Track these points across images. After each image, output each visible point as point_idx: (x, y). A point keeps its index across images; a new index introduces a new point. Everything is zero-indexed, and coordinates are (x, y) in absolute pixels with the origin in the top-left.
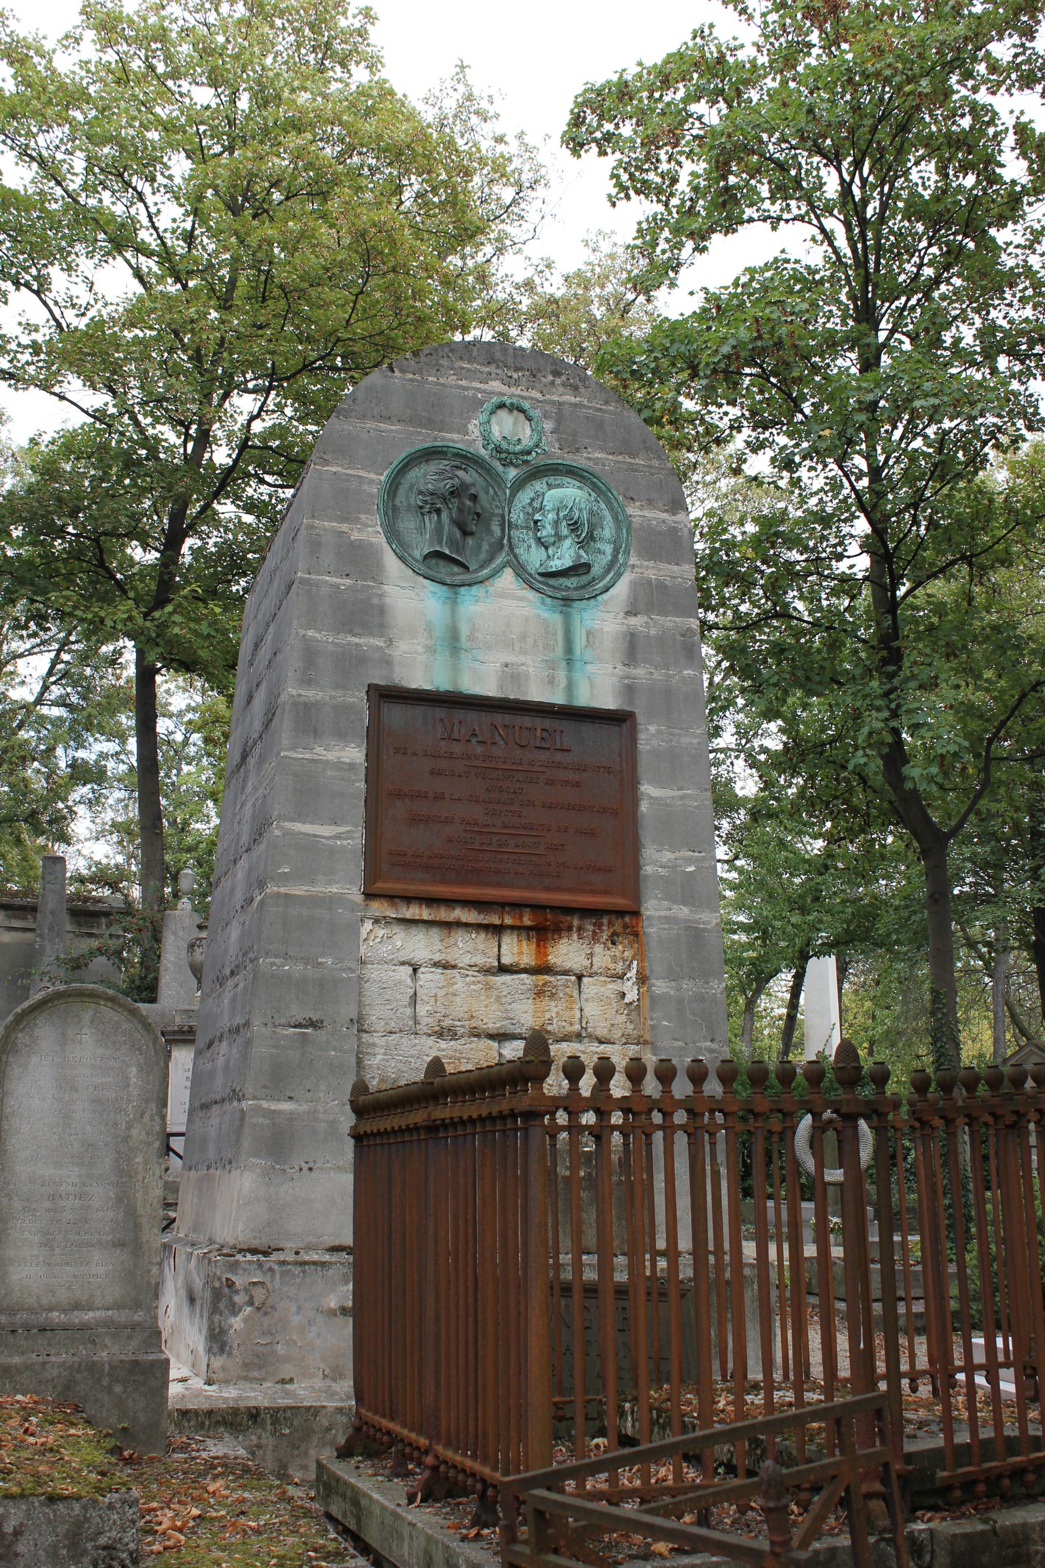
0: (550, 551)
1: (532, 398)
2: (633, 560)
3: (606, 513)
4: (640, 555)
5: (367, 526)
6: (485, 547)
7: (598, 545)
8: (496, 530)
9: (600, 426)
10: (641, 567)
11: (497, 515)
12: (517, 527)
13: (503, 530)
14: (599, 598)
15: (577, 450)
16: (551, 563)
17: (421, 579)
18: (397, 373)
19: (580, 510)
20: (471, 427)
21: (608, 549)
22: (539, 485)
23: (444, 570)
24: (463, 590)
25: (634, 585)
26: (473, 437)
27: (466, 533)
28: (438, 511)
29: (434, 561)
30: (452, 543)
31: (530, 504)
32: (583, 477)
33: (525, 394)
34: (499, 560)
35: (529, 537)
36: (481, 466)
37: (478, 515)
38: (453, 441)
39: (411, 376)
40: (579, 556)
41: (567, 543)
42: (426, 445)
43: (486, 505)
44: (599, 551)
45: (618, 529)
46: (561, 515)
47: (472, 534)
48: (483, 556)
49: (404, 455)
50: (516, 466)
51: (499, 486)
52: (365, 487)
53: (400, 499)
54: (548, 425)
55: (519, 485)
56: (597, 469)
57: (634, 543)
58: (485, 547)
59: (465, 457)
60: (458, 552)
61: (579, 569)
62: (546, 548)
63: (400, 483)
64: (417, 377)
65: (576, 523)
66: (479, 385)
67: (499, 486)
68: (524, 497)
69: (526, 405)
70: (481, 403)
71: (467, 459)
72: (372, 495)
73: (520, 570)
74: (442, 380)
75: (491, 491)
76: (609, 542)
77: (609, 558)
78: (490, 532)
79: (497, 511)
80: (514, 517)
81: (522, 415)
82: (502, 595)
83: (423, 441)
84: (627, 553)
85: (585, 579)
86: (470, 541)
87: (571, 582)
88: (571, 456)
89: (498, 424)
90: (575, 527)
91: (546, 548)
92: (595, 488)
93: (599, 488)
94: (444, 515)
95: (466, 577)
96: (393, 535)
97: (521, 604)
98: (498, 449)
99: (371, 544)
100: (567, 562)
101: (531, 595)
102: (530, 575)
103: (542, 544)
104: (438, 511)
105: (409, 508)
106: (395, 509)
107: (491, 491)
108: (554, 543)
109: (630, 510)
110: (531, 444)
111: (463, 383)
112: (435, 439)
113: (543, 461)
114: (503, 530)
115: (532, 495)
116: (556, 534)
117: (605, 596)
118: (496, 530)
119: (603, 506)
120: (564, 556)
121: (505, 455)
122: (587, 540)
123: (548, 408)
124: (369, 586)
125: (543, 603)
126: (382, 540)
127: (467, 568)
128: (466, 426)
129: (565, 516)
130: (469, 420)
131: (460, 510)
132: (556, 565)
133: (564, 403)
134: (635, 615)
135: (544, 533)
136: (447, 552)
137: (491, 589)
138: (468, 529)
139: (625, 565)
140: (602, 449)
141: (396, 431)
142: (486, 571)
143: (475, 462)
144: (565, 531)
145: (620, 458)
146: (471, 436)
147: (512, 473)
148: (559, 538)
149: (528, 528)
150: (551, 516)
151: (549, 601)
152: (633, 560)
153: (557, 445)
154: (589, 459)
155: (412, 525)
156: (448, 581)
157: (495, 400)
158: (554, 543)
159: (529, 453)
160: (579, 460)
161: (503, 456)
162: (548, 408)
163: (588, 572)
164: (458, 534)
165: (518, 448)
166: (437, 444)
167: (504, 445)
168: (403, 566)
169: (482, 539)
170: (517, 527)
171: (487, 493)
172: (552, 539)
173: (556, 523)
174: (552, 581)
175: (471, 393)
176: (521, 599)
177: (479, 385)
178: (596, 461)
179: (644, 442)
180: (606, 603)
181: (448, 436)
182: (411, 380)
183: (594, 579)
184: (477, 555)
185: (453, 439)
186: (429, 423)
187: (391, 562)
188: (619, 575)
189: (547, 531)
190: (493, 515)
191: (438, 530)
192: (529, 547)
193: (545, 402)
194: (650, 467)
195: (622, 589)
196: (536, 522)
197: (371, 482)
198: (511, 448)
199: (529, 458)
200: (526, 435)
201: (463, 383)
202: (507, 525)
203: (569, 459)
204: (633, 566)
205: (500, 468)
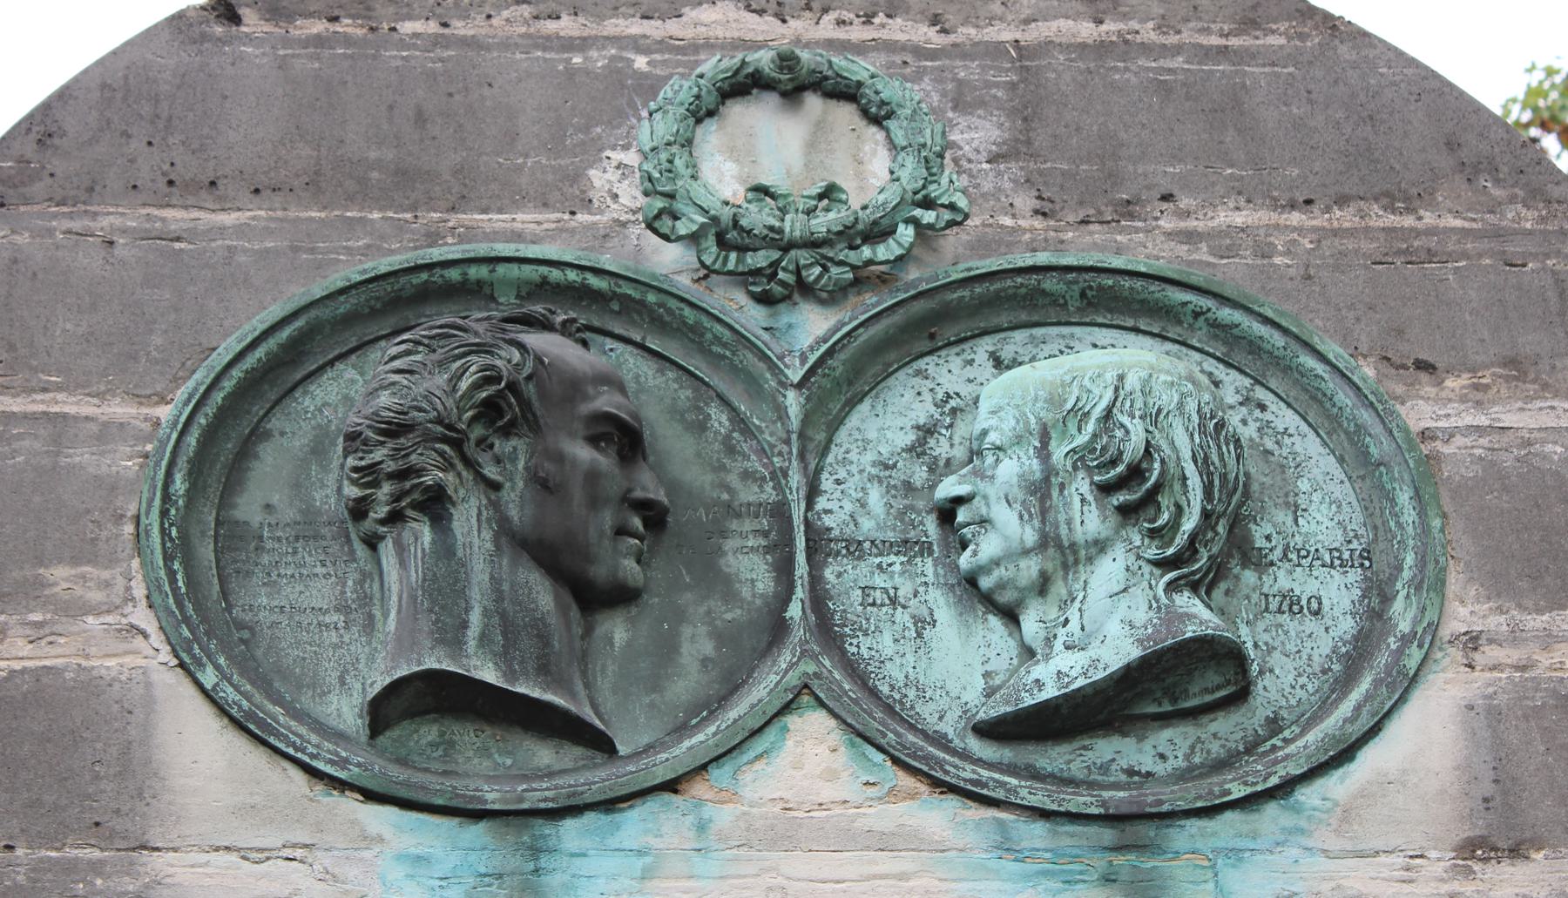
0: (1031, 625)
1: (891, 47)
2: (1465, 612)
3: (1309, 446)
4: (1500, 585)
5: (76, 609)
6: (696, 645)
7: (1282, 579)
8: (752, 571)
9: (1228, 108)
10: (1516, 636)
11: (755, 510)
12: (855, 548)
13: (784, 569)
14: (1308, 795)
15: (1128, 209)
16: (1040, 671)
17: (350, 805)
18: (252, 21)
19: (1154, 418)
20: (600, 179)
21: (1339, 593)
22: (948, 372)
23: (491, 765)
24: (570, 831)
25: (1487, 719)
26: (615, 211)
27: (594, 597)
28: (435, 504)
29: (428, 732)
30: (510, 631)
31: (917, 450)
32: (1169, 313)
33: (858, 33)
34: (763, 689)
35: (925, 585)
36: (660, 324)
37: (654, 517)
38: (517, 236)
39: (319, 27)
40: (1173, 617)
41: (1109, 571)
42: (384, 265)
43: (698, 478)
44: (1291, 604)
45: (1376, 500)
46: (1059, 452)
47: (622, 596)
48: (686, 683)
49: (275, 312)
50: (833, 297)
51: (753, 385)
52: (82, 456)
53: (265, 493)
54: (977, 135)
55: (846, 379)
56: (1233, 273)
57: (1463, 544)
58: (696, 645)
59: (581, 294)
60: (545, 670)
61: (1178, 680)
62: (1011, 616)
63: (258, 434)
64: (346, 26)
65: (1135, 473)
66: (636, 27)
67: (753, 385)
68: (885, 424)
69: (858, 69)
70: (649, 87)
71: (591, 299)
72: (112, 486)
73: (884, 728)
74: (460, 28)
75: (719, 419)
76: (1338, 561)
77: (1347, 626)
78: (716, 581)
79: (749, 494)
80: (835, 511)
81: (845, 113)
82: (785, 831)
83: (366, 252)
84: (1431, 583)
85: (1226, 729)
86: (617, 630)
87: (1153, 754)
88: (1097, 234)
89: (732, 152)
90: (1133, 489)
91: (1011, 616)
92: (1234, 348)
93: (1255, 347)
94: (468, 518)
95: (599, 778)
96: (210, 623)
97: (887, 863)
98: (728, 234)
99: (91, 686)
100: (1116, 649)
101: (939, 817)
102: (940, 741)
103: (989, 601)
104: (435, 504)
105: (307, 530)
106: (231, 536)
107: (719, 419)
108: (1042, 586)
109: (1420, 411)
110: (892, 196)
111: (567, 26)
112: (433, 238)
113: (956, 258)
114: (784, 569)
115: (923, 411)
116: (1047, 541)
117: (1337, 785)
118: (752, 571)
119: (1285, 418)
120: (1110, 617)
121: (769, 258)
122: (1215, 552)
123: (968, 71)
124: (70, 868)
125: (1006, 847)
126: (152, 657)
127: (601, 744)
128: (577, 177)
129: (1079, 458)
130: (593, 152)
131: (543, 485)
132: (1061, 672)
133: (1047, 46)
134: (1516, 852)
135: (988, 547)
136: (489, 674)
137: (723, 816)
138: (599, 572)
139: (1428, 636)
140: (1248, 195)
141: (241, 230)
142: (703, 739)
143: (631, 308)
144: (1085, 516)
145: (1344, 217)
146: (603, 214)
147: (811, 326)
148: (1065, 556)
149: (910, 547)
150: (1011, 469)
151: (1035, 833)
152: (1465, 612)
153: (1025, 201)
154: (1190, 237)
155: (320, 593)
156: (493, 797)
157: (713, 66)
158: (1042, 586)
159: (878, 232)
160: (1143, 248)
161: (759, 259)
162: (968, 71)
163: (1241, 696)
164: (543, 595)
165: (824, 222)
166: (436, 254)
167: (759, 217)
168: (256, 758)
169: (680, 616)
170: (855, 548)
171: (701, 427)
172: (1030, 569)
173: (1040, 493)
174: (1054, 758)
175: (599, 59)
176: (885, 843)
177: (636, 27)
178: (1226, 242)
179: (1452, 145)
180: (1347, 814)
181: (497, 220)
182: (319, 41)
183: (1274, 725)
184: (655, 684)
185: (529, 231)
186: (406, 184)
187: (196, 750)
188: (1403, 685)
189: (1002, 534)
190: (732, 511)
191: (442, 596)
192: (923, 623)
193: (957, 51)
194: (1498, 234)
195: (1425, 741)
196: (946, 513)
197: (108, 433)
198: (793, 225)
199: (885, 251)
200: (871, 172)
201: (567, 26)
202: (800, 544)
203: (1086, 246)
204: (1472, 641)
205: (751, 317)
